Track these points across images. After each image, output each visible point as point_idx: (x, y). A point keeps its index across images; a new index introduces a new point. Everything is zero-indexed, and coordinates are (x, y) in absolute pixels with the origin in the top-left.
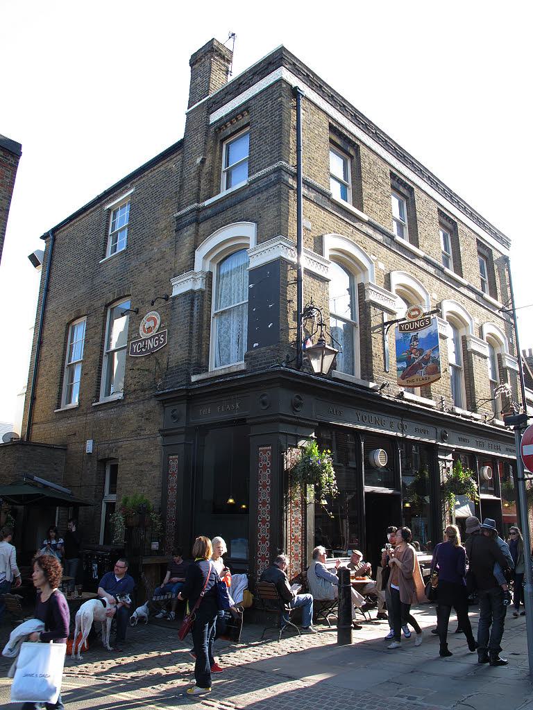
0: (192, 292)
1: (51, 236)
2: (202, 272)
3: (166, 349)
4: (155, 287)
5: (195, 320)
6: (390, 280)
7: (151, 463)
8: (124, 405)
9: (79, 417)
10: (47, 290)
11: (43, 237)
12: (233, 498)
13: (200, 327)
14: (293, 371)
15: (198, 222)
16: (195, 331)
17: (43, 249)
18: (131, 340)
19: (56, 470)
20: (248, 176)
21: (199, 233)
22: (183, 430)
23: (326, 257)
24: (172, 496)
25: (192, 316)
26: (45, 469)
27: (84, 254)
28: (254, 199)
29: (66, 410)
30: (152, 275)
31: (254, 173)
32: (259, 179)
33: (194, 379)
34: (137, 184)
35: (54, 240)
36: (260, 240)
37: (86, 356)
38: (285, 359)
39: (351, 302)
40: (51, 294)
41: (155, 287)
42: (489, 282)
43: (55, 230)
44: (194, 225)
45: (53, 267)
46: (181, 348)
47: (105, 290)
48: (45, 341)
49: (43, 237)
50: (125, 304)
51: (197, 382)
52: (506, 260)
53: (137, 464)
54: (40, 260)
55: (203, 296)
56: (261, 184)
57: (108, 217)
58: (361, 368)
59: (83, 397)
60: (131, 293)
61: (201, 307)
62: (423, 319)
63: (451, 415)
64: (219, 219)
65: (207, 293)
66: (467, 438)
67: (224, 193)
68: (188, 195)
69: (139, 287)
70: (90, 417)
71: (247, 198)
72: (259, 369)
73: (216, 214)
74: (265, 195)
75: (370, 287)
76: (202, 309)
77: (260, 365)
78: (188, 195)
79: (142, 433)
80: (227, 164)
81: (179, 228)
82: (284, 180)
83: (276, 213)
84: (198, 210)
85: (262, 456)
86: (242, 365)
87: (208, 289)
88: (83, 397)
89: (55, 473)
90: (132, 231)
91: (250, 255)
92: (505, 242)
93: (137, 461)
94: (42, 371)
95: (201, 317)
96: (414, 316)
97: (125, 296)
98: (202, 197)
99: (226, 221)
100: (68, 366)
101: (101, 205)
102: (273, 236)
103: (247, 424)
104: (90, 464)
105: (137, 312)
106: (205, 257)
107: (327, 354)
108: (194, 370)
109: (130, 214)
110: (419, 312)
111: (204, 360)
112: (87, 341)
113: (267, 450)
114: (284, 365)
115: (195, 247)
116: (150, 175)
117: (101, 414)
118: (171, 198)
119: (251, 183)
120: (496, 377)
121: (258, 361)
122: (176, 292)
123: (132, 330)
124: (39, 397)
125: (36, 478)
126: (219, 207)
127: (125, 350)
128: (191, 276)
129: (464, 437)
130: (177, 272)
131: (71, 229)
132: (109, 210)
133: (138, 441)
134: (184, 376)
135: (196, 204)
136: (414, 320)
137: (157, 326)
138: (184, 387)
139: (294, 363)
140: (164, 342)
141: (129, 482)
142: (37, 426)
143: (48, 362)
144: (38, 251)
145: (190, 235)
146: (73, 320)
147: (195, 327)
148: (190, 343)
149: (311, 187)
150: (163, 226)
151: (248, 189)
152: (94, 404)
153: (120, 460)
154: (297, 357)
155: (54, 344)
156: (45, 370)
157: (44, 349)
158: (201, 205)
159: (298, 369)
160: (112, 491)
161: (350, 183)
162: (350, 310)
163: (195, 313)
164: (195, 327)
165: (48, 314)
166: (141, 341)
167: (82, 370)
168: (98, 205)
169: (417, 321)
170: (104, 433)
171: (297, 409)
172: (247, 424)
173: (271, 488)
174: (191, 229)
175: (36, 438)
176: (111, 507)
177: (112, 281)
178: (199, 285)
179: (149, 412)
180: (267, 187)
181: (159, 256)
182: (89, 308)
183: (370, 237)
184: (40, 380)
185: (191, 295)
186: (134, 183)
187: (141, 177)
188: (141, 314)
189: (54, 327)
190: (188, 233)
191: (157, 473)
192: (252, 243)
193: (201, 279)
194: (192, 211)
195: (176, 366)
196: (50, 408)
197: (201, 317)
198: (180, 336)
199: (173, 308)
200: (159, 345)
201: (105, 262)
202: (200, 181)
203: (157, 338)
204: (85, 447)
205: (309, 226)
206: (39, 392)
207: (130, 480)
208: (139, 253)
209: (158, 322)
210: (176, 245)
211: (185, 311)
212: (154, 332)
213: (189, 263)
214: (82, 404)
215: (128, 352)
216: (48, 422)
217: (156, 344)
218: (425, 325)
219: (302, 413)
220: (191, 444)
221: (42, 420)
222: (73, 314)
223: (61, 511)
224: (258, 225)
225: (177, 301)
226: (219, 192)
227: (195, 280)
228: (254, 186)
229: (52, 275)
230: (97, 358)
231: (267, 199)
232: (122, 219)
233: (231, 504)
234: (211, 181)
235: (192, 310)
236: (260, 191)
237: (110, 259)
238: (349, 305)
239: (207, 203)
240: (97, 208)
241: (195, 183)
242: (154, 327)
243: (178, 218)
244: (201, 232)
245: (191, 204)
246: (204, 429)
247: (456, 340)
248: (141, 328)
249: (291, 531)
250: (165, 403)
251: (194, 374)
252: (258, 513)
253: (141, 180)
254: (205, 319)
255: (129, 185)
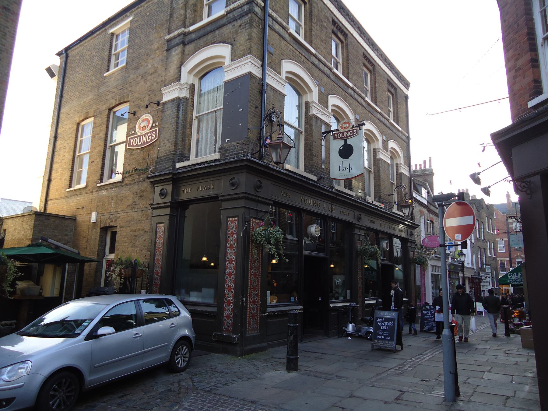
0: (178, 99)
1: (65, 53)
2: (186, 83)
3: (157, 143)
4: (149, 95)
5: (180, 121)
6: (328, 101)
7: (143, 230)
8: (122, 186)
9: (86, 195)
10: (61, 96)
11: (59, 54)
12: (206, 257)
13: (184, 127)
14: (255, 160)
15: (184, 44)
16: (180, 130)
17: (59, 65)
18: (129, 136)
19: (66, 235)
20: (226, 7)
21: (185, 53)
22: (169, 204)
23: (284, 75)
24: (159, 255)
25: (178, 117)
26: (57, 234)
27: (92, 68)
28: (230, 26)
29: (76, 190)
30: (147, 86)
31: (230, 5)
32: (234, 9)
33: (178, 165)
34: (134, 13)
35: (67, 57)
36: (234, 57)
37: (93, 148)
38: (250, 151)
39: (299, 115)
40: (64, 100)
41: (149, 95)
42: (394, 112)
43: (67, 49)
44: (181, 45)
45: (66, 78)
46: (169, 142)
47: (109, 97)
48: (59, 136)
49: (59, 54)
50: (123, 109)
51: (182, 168)
52: (406, 97)
53: (131, 231)
54: (56, 72)
55: (187, 103)
56: (235, 13)
57: (112, 39)
58: (304, 164)
59: (90, 179)
60: (129, 99)
61: (185, 111)
62: (352, 130)
63: (364, 203)
64: (202, 42)
65: (190, 100)
66: (374, 220)
67: (206, 20)
68: (177, 22)
69: (137, 95)
70: (95, 195)
71: (224, 25)
72: (230, 158)
73: (199, 38)
74: (239, 22)
75: (314, 105)
76: (186, 113)
77: (231, 155)
78: (177, 22)
79: (136, 207)
80: (198, 112)
81: (170, 46)
82: (254, 11)
83: (247, 37)
84: (185, 34)
85: (231, 225)
86: (217, 156)
87: (191, 97)
88: (90, 179)
89: (66, 237)
90: (131, 51)
91: (225, 70)
92: (407, 84)
93: (132, 228)
94: (56, 159)
95: (185, 119)
96: (345, 128)
97: (125, 102)
98: (187, 23)
99: (207, 44)
100: (79, 156)
101: (106, 29)
102: (244, 55)
103: (219, 200)
104: (94, 230)
105: (134, 114)
106: (190, 72)
107: (283, 148)
108: (179, 159)
109: (130, 37)
110: (349, 125)
111: (186, 152)
112: (93, 137)
113: (234, 220)
114: (249, 155)
115: (182, 64)
116: (146, 6)
117: (104, 193)
118: (163, 25)
119: (228, 13)
120: (394, 180)
121: (229, 153)
122: (165, 99)
123: (131, 132)
124: (54, 179)
125: (50, 240)
126: (201, 32)
127: (124, 144)
128: (178, 86)
129: (372, 220)
130: (166, 83)
131: (82, 48)
132: (113, 34)
133: (133, 213)
134: (171, 164)
135: (183, 29)
136: (346, 130)
137: (150, 125)
138: (171, 172)
139: (257, 155)
140: (155, 138)
141: (125, 244)
142: (53, 201)
143: (62, 153)
144: (54, 65)
145: (177, 54)
146: (83, 120)
147: (180, 127)
148: (176, 138)
149: (275, 21)
150: (156, 47)
151: (225, 18)
152: (98, 185)
153: (118, 227)
154: (260, 150)
155: (66, 138)
156: (59, 159)
157: (58, 143)
158: (187, 30)
159: (260, 159)
160: (112, 251)
161: (302, 23)
162: (298, 121)
163: (180, 116)
164: (180, 127)
165: (61, 115)
166: (137, 137)
167: (90, 158)
168: (103, 29)
169: (347, 132)
170: (106, 207)
171: (259, 190)
172: (219, 200)
173: (237, 249)
174: (179, 49)
175: (49, 211)
176: (110, 263)
177: (115, 90)
178: (185, 94)
179: (143, 191)
180: (241, 16)
181: (152, 71)
182: (95, 111)
183: (316, 66)
184: (55, 166)
185: (178, 101)
186: (132, 12)
187: (139, 8)
188: (137, 115)
189: (67, 127)
190: (176, 53)
191: (147, 237)
192: (227, 61)
193: (186, 89)
194: (179, 35)
195: (164, 156)
196: (63, 187)
197: (185, 119)
198: (169, 132)
199: (163, 111)
200: (152, 140)
201: (109, 76)
202: (186, 11)
203: (150, 134)
204: (90, 218)
205: (272, 50)
206: (54, 175)
207: (126, 243)
208: (137, 68)
209: (151, 122)
210: (166, 61)
211: (173, 113)
212: (147, 130)
213: (176, 76)
214: (90, 184)
215: (126, 145)
216: (61, 198)
217: (149, 139)
218: (353, 135)
219: (262, 193)
220: (175, 216)
221: (57, 197)
222: (83, 116)
223: (70, 267)
224: (232, 47)
225: (166, 106)
226: (201, 20)
227: (181, 89)
228: (230, 15)
229: (65, 85)
230: (102, 149)
231: (241, 26)
232: (123, 42)
233: (204, 261)
234: (195, 11)
235: (178, 112)
236: (234, 19)
237: (113, 73)
238: (297, 118)
239: (192, 28)
240: (102, 32)
241: (182, 12)
242: (148, 126)
243: (168, 41)
244: (187, 52)
245: (178, 29)
246: (185, 204)
247: (369, 151)
248: (137, 127)
249: (251, 282)
250: (155, 184)
251: (178, 162)
252: (225, 268)
253: (139, 10)
254: (188, 120)
255: (128, 14)
